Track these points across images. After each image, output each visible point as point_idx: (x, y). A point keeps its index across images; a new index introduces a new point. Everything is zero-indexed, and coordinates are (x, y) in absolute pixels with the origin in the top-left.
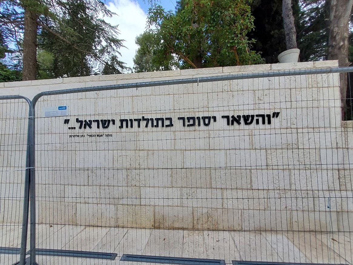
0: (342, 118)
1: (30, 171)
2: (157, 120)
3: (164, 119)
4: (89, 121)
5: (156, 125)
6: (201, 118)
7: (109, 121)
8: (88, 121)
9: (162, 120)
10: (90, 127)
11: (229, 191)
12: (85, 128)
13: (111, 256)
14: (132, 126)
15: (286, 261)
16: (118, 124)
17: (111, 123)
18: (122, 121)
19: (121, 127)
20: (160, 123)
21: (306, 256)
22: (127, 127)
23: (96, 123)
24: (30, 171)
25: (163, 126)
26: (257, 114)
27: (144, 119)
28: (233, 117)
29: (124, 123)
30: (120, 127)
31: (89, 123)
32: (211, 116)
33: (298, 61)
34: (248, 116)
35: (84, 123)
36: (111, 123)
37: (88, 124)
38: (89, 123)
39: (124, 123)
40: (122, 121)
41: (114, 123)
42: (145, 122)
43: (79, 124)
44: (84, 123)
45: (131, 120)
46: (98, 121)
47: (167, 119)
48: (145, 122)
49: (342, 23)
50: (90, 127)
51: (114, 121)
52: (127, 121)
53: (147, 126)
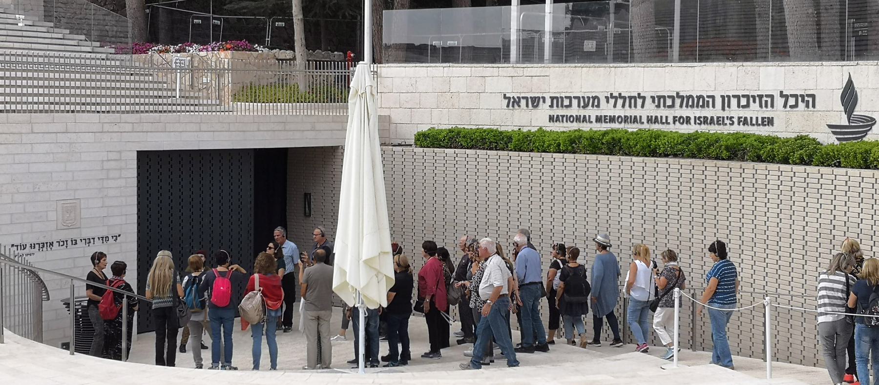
0: (343, 154)
1: (843, 50)
7: (539, 98)
9: (664, 97)
11: (288, 57)
14: (635, 106)
17: (541, 100)
18: (552, 98)
19: (551, 106)
23: (577, 101)
24: (843, 50)
27: (620, 96)
36: (541, 100)
40: (552, 98)
41: (544, 102)
42: (613, 100)
43: (507, 101)
45: (728, 97)
46: (526, 98)
51: (544, 98)
52: (557, 98)
53: (623, 106)
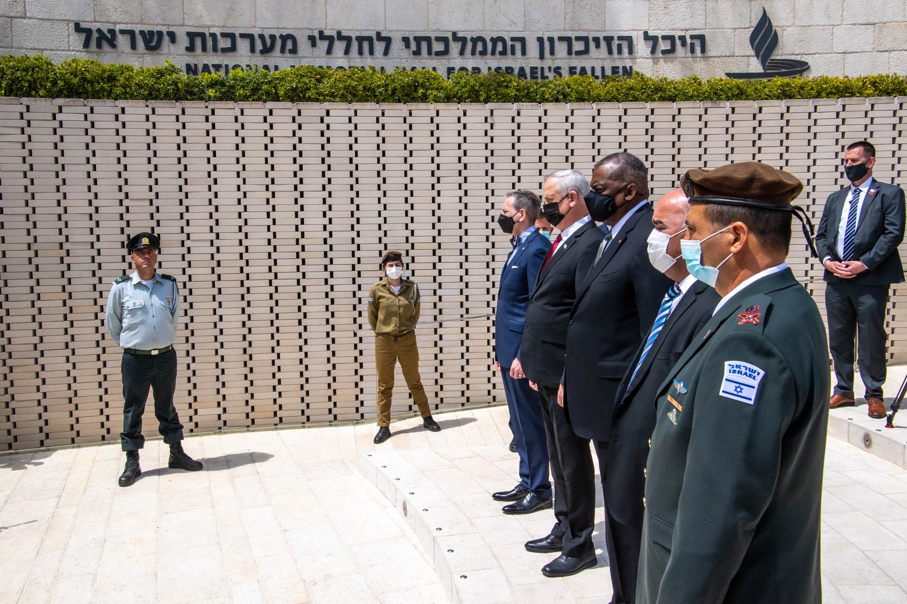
2: (418, 40)
3: (238, 36)
4: (110, 31)
5: (291, 48)
6: (591, 39)
7: (160, 34)
8: (105, 31)
9: (428, 39)
10: (113, 46)
12: (99, 46)
14: (371, 52)
15: (128, 343)
16: (184, 42)
17: (166, 39)
18: (191, 36)
19: (191, 49)
20: (424, 45)
21: (897, 585)
22: (204, 49)
25: (430, 53)
27: (340, 36)
28: (99, 31)
29: (198, 42)
30: (187, 49)
31: (109, 36)
32: (469, 38)
34: (151, 33)
35: (95, 35)
36: (166, 39)
38: (109, 36)
39: (198, 42)
40: (191, 36)
45: (551, 40)
46: (131, 33)
47: (578, 39)
50: (113, 46)
51: (172, 36)
52: (202, 36)
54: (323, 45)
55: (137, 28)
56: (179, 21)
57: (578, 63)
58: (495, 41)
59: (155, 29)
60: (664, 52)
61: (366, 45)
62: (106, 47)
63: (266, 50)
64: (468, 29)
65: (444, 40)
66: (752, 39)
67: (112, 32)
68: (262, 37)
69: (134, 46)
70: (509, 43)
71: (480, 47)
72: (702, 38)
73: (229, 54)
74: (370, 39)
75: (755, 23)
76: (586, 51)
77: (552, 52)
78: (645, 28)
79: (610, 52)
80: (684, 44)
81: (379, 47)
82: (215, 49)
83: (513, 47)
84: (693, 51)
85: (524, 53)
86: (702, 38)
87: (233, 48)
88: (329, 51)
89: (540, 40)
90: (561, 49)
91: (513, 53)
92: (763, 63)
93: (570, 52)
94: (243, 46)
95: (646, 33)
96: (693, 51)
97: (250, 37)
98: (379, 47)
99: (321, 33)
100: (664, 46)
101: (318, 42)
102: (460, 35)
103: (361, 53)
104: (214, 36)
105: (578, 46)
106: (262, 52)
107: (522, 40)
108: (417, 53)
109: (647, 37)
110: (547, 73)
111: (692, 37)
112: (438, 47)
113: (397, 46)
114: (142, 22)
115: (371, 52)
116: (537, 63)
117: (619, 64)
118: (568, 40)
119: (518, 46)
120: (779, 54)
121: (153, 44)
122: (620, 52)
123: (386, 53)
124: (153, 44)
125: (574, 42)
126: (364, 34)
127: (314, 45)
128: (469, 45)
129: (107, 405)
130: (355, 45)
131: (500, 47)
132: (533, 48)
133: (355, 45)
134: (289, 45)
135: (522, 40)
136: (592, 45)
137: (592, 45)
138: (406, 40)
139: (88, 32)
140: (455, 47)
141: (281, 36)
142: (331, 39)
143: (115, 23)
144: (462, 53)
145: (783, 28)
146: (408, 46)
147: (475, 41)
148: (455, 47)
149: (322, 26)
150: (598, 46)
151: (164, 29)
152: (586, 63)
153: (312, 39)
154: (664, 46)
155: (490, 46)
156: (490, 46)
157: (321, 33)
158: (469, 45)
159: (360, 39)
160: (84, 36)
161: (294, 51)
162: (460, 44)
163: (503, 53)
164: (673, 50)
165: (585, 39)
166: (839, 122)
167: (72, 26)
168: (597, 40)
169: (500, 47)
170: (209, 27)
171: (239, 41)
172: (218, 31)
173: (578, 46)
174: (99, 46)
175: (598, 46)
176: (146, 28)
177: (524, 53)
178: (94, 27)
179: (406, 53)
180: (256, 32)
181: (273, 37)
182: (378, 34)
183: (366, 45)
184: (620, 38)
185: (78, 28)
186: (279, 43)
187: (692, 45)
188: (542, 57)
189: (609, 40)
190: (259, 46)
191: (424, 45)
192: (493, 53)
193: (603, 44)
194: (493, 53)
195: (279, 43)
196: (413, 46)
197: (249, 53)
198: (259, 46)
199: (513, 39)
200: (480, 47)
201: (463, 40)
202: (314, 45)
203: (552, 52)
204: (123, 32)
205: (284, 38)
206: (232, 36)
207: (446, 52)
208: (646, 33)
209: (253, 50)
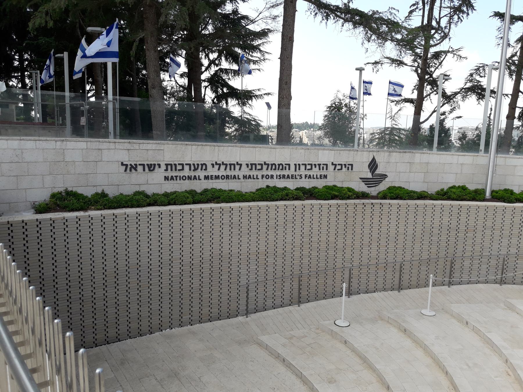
2: (252, 165)
4: (135, 164)
7: (155, 165)
9: (255, 164)
10: (136, 170)
12: (131, 170)
13: (477, 195)
14: (234, 169)
16: (163, 167)
17: (157, 166)
18: (167, 165)
19: (166, 170)
20: (254, 166)
22: (172, 170)
23: (304, 166)
25: (256, 169)
26: (215, 159)
27: (265, 163)
28: (131, 165)
29: (169, 167)
33: (89, 46)
34: (151, 165)
35: (129, 167)
36: (157, 166)
37: (134, 168)
39: (169, 167)
40: (167, 165)
42: (224, 166)
44: (129, 167)
45: (299, 165)
46: (144, 165)
48: (224, 166)
49: (261, 39)
50: (136, 170)
51: (159, 165)
52: (171, 165)
54: (217, 167)
55: (145, 163)
56: (162, 159)
57: (308, 173)
58: (279, 165)
59: (153, 163)
60: (338, 170)
61: (232, 167)
62: (133, 170)
63: (195, 169)
64: (270, 161)
65: (262, 165)
66: (369, 166)
67: (136, 165)
68: (194, 164)
69: (144, 170)
70: (284, 166)
71: (274, 167)
72: (352, 165)
73: (181, 171)
74: (234, 165)
75: (370, 160)
76: (311, 169)
77: (299, 169)
78: (332, 161)
79: (320, 169)
80: (345, 167)
81: (237, 167)
82: (176, 170)
83: (285, 167)
84: (348, 169)
85: (289, 169)
86: (352, 165)
87: (183, 169)
88: (219, 169)
89: (295, 165)
90: (303, 168)
91: (285, 169)
92: (372, 175)
93: (305, 169)
94: (187, 168)
95: (332, 163)
96: (348, 169)
97: (190, 165)
98: (237, 167)
99: (216, 162)
100: (339, 167)
101: (215, 165)
102: (267, 163)
103: (230, 169)
104: (175, 165)
105: (309, 167)
106: (194, 170)
107: (289, 165)
108: (251, 169)
109: (333, 164)
110: (297, 177)
111: (348, 165)
112: (259, 167)
113: (244, 167)
114: (148, 160)
115: (234, 169)
116: (294, 173)
117: (323, 174)
118: (305, 165)
119: (287, 167)
120: (378, 172)
121: (152, 169)
122: (323, 169)
123: (240, 169)
124: (152, 169)
125: (307, 166)
126: (232, 163)
127: (213, 167)
128: (270, 166)
129: (26, 230)
130: (228, 167)
131: (281, 167)
132: (293, 167)
133: (228, 167)
134: (204, 167)
135: (289, 165)
136: (313, 166)
137: (313, 166)
138: (247, 165)
139: (127, 165)
140: (265, 167)
141: (201, 164)
142: (220, 165)
143: (137, 161)
144: (267, 169)
145: (380, 163)
146: (248, 167)
147: (272, 165)
148: (265, 167)
149: (216, 160)
150: (315, 167)
151: (156, 163)
152: (311, 173)
153: (213, 165)
154: (339, 167)
155: (277, 166)
156: (277, 166)
157: (216, 162)
158: (270, 166)
159: (230, 165)
160: (124, 167)
161: (206, 169)
162: (267, 166)
163: (282, 169)
164: (341, 169)
165: (311, 165)
166: (485, 220)
167: (120, 163)
168: (315, 165)
169: (281, 167)
170: (174, 161)
171: (185, 166)
172: (177, 163)
173: (309, 167)
174: (131, 170)
175: (315, 167)
176: (149, 163)
177: (289, 169)
178: (129, 163)
179: (247, 169)
180: (191, 163)
181: (198, 165)
182: (237, 163)
183: (232, 167)
184: (323, 164)
185: (122, 164)
186: (200, 166)
187: (348, 167)
188: (296, 171)
189: (319, 165)
190: (192, 168)
191: (254, 166)
192: (278, 169)
193: (317, 166)
194: (278, 169)
195: (200, 166)
196: (250, 167)
197: (188, 170)
198: (192, 168)
199: (286, 164)
200: (274, 167)
201: (268, 165)
202: (213, 167)
203: (299, 169)
204: (140, 165)
205: (202, 165)
206: (182, 165)
207: (262, 169)
208: (332, 163)
209: (190, 170)
